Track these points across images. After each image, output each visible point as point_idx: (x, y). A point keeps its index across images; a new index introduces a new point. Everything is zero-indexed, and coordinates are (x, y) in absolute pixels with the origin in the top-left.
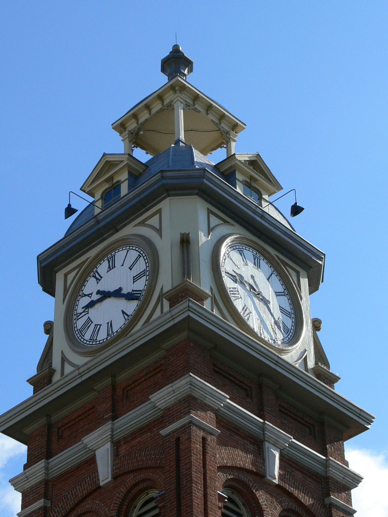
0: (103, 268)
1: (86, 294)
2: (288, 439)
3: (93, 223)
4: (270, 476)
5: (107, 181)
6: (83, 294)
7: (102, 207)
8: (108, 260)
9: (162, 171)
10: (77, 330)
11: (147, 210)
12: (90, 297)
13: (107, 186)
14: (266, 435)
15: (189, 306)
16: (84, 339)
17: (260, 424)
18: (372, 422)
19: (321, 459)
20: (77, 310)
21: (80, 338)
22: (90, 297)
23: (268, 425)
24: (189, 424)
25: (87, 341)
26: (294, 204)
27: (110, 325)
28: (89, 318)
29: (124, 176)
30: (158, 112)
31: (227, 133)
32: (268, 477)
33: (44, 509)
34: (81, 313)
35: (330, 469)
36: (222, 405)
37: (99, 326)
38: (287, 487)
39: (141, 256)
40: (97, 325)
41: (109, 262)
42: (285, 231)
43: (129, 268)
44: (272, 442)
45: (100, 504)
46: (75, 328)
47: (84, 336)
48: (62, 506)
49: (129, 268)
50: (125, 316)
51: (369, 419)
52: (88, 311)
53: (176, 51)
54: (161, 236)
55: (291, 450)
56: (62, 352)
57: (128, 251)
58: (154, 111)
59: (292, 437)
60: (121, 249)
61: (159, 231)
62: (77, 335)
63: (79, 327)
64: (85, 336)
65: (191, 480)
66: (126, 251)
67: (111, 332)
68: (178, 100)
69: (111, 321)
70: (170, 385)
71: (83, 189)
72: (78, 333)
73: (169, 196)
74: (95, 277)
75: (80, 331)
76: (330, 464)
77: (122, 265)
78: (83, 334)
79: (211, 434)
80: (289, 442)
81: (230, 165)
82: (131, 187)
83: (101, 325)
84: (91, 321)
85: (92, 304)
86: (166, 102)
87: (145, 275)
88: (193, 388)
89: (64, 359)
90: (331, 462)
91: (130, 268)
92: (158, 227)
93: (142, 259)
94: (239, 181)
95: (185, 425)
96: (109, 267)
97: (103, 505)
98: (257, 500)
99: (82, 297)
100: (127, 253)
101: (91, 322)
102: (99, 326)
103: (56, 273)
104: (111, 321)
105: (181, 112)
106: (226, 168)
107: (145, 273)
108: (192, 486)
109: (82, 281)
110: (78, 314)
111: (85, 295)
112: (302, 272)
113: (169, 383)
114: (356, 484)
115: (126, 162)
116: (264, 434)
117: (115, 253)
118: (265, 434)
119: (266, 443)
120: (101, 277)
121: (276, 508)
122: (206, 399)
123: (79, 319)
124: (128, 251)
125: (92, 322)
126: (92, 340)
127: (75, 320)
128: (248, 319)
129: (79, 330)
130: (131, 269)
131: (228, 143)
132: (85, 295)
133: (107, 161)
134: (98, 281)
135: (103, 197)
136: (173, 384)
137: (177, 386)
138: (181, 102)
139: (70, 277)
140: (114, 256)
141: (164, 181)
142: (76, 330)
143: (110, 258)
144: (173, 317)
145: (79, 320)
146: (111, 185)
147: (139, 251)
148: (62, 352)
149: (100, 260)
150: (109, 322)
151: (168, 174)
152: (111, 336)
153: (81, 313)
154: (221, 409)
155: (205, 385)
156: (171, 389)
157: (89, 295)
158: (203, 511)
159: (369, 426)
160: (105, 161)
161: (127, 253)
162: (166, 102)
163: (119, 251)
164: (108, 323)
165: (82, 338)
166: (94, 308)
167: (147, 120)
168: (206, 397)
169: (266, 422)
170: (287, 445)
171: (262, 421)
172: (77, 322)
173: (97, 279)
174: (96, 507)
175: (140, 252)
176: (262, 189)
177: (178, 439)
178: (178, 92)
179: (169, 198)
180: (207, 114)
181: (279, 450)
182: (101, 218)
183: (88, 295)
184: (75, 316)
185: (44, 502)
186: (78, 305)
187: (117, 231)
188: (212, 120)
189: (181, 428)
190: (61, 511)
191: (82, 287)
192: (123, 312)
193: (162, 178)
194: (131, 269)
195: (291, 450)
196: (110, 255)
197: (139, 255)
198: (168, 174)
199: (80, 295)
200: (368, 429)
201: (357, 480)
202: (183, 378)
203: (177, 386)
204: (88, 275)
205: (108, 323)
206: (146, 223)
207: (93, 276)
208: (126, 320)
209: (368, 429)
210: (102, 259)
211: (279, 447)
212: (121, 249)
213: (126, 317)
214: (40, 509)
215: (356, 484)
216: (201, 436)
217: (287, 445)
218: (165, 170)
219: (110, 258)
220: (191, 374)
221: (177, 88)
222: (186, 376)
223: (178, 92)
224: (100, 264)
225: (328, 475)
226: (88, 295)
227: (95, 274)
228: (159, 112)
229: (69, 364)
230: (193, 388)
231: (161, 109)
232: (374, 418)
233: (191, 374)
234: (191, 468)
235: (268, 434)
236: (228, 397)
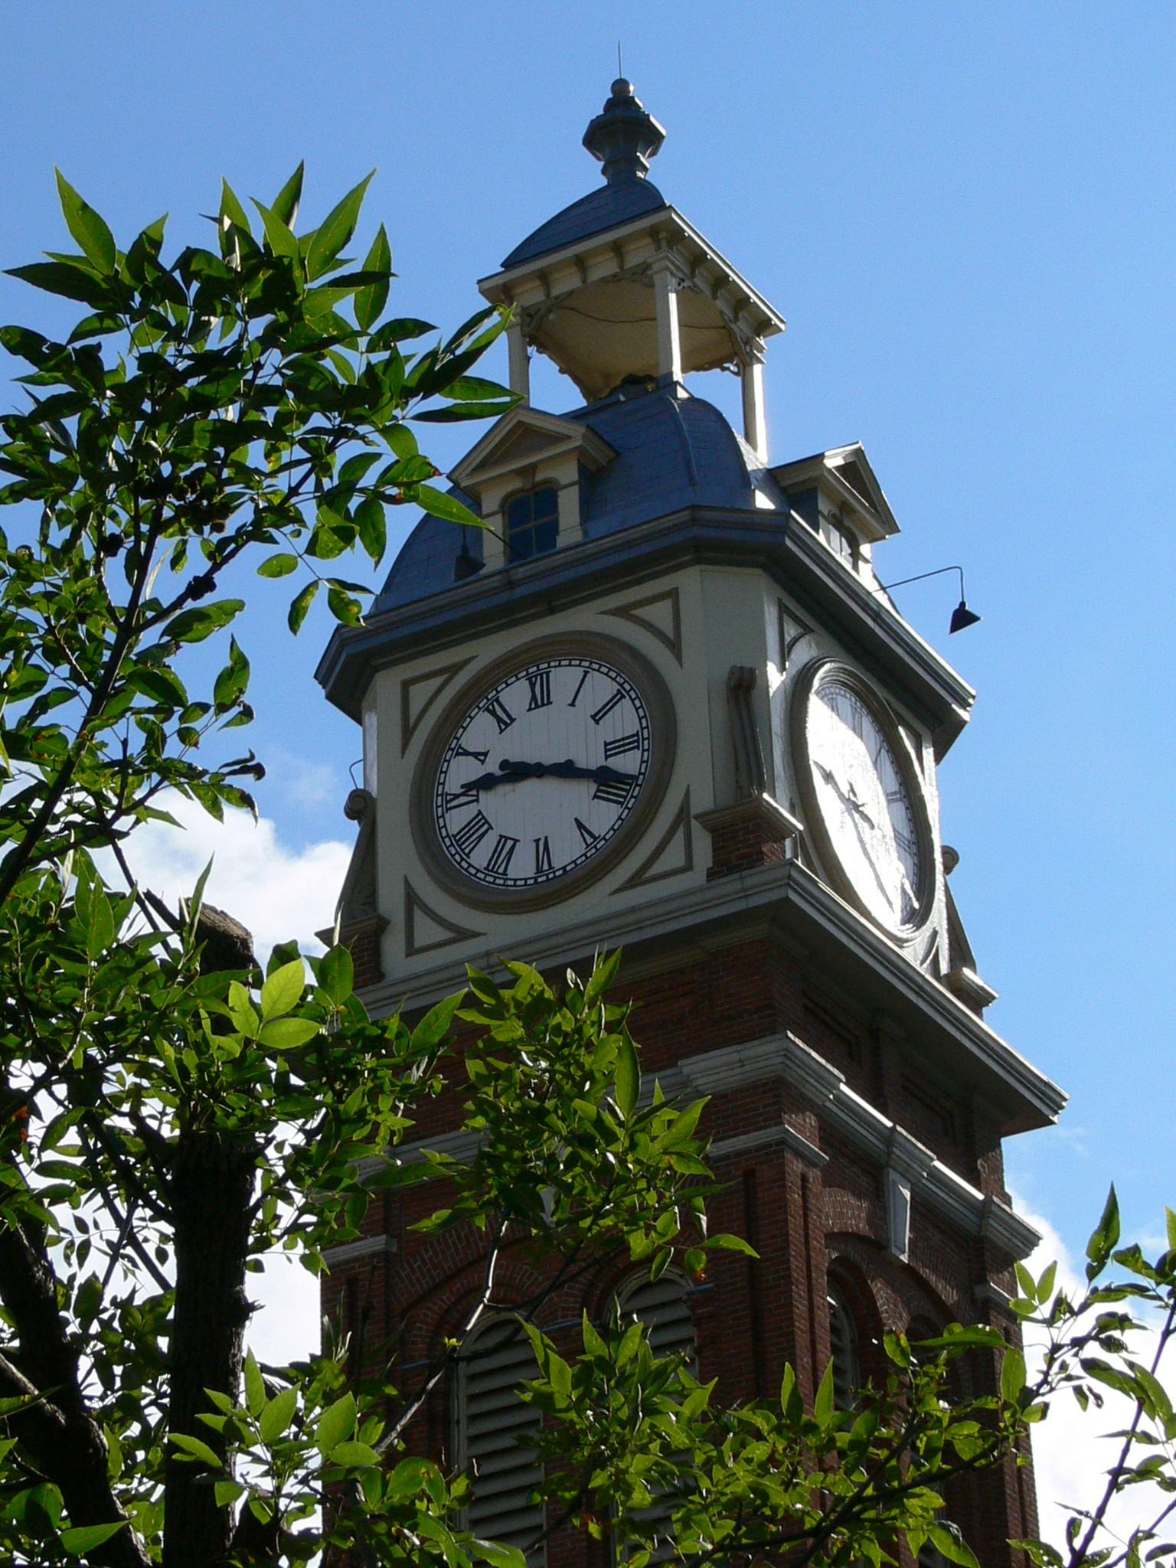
0: (515, 695)
1: (471, 750)
2: (928, 1161)
3: (496, 584)
4: (897, 1247)
5: (519, 472)
6: (460, 747)
7: (503, 533)
8: (530, 679)
9: (694, 507)
10: (448, 836)
11: (639, 581)
12: (483, 762)
13: (516, 484)
14: (894, 1156)
15: (790, 877)
16: (470, 865)
17: (885, 1130)
18: (1062, 1108)
19: (880, 1127)
20: (443, 784)
21: (457, 857)
22: (483, 762)
23: (900, 1133)
24: (777, 1144)
25: (478, 871)
26: (957, 607)
27: (543, 847)
28: (480, 813)
29: (567, 473)
30: (605, 281)
31: (746, 344)
32: (894, 1250)
33: (385, 1256)
34: (456, 796)
35: (991, 1222)
36: (831, 1097)
37: (510, 843)
38: (926, 1273)
39: (623, 697)
40: (507, 838)
41: (532, 686)
42: (877, 613)
43: (593, 717)
44: (901, 1170)
45: (531, 1274)
46: (440, 828)
47: (468, 855)
48: (430, 1259)
49: (593, 717)
50: (586, 835)
51: (1054, 1101)
52: (477, 795)
53: (621, 99)
54: (679, 658)
55: (930, 1186)
56: (406, 881)
57: (586, 673)
58: (596, 274)
59: (935, 1157)
60: (567, 662)
61: (674, 645)
62: (447, 848)
63: (454, 829)
64: (471, 855)
65: (789, 1276)
66: (580, 671)
67: (546, 867)
68: (667, 268)
69: (546, 838)
70: (735, 1047)
71: (454, 477)
72: (452, 844)
73: (698, 561)
74: (493, 713)
75: (458, 840)
76: (991, 1212)
77: (572, 704)
78: (467, 851)
79: (815, 1165)
80: (929, 1166)
81: (805, 477)
82: (588, 507)
83: (516, 841)
84: (487, 822)
85: (487, 783)
86: (633, 260)
87: (622, 803)
88: (788, 1062)
89: (412, 899)
90: (994, 1208)
91: (596, 718)
92: (670, 632)
93: (627, 701)
94: (823, 516)
95: (769, 1145)
96: (534, 698)
97: (540, 1278)
98: (872, 1299)
99: (458, 754)
100: (585, 676)
101: (486, 827)
102: (510, 843)
103: (377, 671)
104: (546, 838)
105: (673, 298)
106: (797, 480)
107: (637, 741)
108: (791, 1290)
109: (456, 716)
110: (447, 794)
111: (466, 753)
112: (926, 735)
113: (727, 1042)
114: (1026, 1249)
115: (578, 444)
116: (890, 1154)
117: (549, 667)
118: (893, 1152)
119: (891, 1171)
120: (512, 720)
121: (901, 1316)
122: (807, 1085)
123: (451, 808)
124: (586, 673)
125: (491, 828)
126: (492, 871)
127: (440, 809)
128: (961, 952)
129: (454, 836)
130: (597, 722)
131: (747, 368)
132: (466, 753)
133: (519, 422)
134: (503, 727)
135: (506, 508)
136: (740, 1047)
137: (751, 1053)
138: (672, 273)
139: (420, 694)
140: (548, 673)
141: (695, 531)
142: (444, 834)
143: (536, 676)
144: (748, 893)
145: (453, 811)
146: (528, 486)
147: (618, 679)
148: (406, 881)
149: (508, 674)
150: (539, 839)
151: (708, 515)
152: (547, 875)
153: (456, 796)
154: (828, 1104)
155: (809, 1055)
156: (735, 1057)
157: (481, 756)
158: (809, 1345)
159: (1055, 1119)
160: (514, 422)
161: (585, 676)
162: (633, 260)
163: (559, 665)
164: (537, 841)
165: (462, 859)
166: (493, 791)
167: (572, 292)
168: (807, 1081)
169: (899, 1128)
170: (925, 1174)
171: (889, 1124)
172: (447, 816)
173: (499, 720)
174: (521, 1279)
175: (621, 685)
176: (861, 531)
177: (749, 1174)
178: (664, 244)
179: (698, 567)
180: (715, 297)
181: (909, 1186)
182: (520, 576)
183: (476, 755)
184: (440, 798)
185: (387, 1243)
186: (446, 772)
187: (552, 611)
188: (721, 312)
189: (758, 1148)
190: (429, 1271)
191: (456, 728)
192: (580, 826)
193: (694, 521)
194: (597, 722)
195: (930, 1186)
196: (535, 668)
197: (619, 692)
198: (708, 515)
199: (453, 750)
200: (1052, 1123)
201: (1027, 1239)
202: (769, 1038)
203: (751, 1053)
204: (474, 703)
205: (537, 841)
206: (633, 612)
207: (487, 710)
208: (588, 846)
209: (1052, 1123)
210: (513, 672)
211: (911, 1179)
212: (567, 662)
213: (589, 840)
214: (373, 1255)
215: (1026, 1249)
216: (799, 1171)
217: (925, 1174)
218: (702, 504)
219: (536, 676)
220: (790, 1035)
221: (663, 235)
222: (778, 1036)
223: (664, 244)
224: (506, 682)
225: (983, 1234)
226: (476, 755)
227: (492, 704)
228: (608, 282)
229: (425, 913)
230: (788, 1062)
231: (615, 276)
232: (1065, 1100)
233: (790, 1035)
234: (787, 1247)
235: (898, 1152)
236: (842, 1077)
